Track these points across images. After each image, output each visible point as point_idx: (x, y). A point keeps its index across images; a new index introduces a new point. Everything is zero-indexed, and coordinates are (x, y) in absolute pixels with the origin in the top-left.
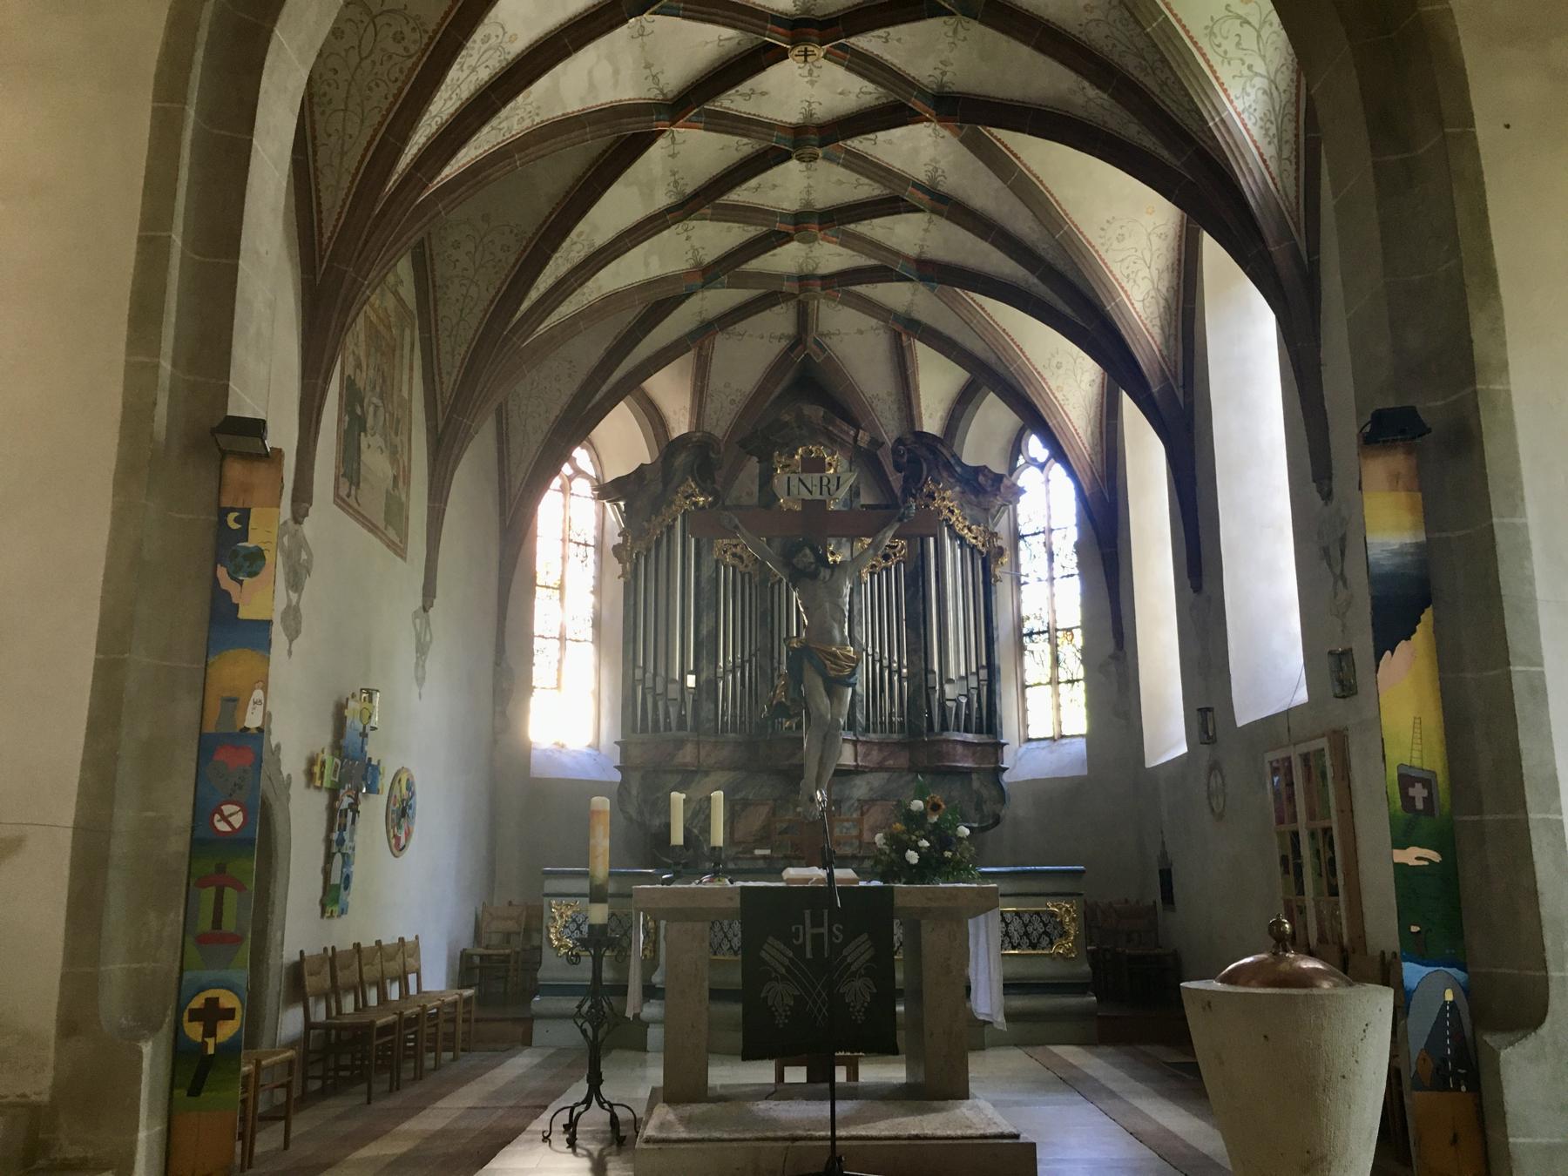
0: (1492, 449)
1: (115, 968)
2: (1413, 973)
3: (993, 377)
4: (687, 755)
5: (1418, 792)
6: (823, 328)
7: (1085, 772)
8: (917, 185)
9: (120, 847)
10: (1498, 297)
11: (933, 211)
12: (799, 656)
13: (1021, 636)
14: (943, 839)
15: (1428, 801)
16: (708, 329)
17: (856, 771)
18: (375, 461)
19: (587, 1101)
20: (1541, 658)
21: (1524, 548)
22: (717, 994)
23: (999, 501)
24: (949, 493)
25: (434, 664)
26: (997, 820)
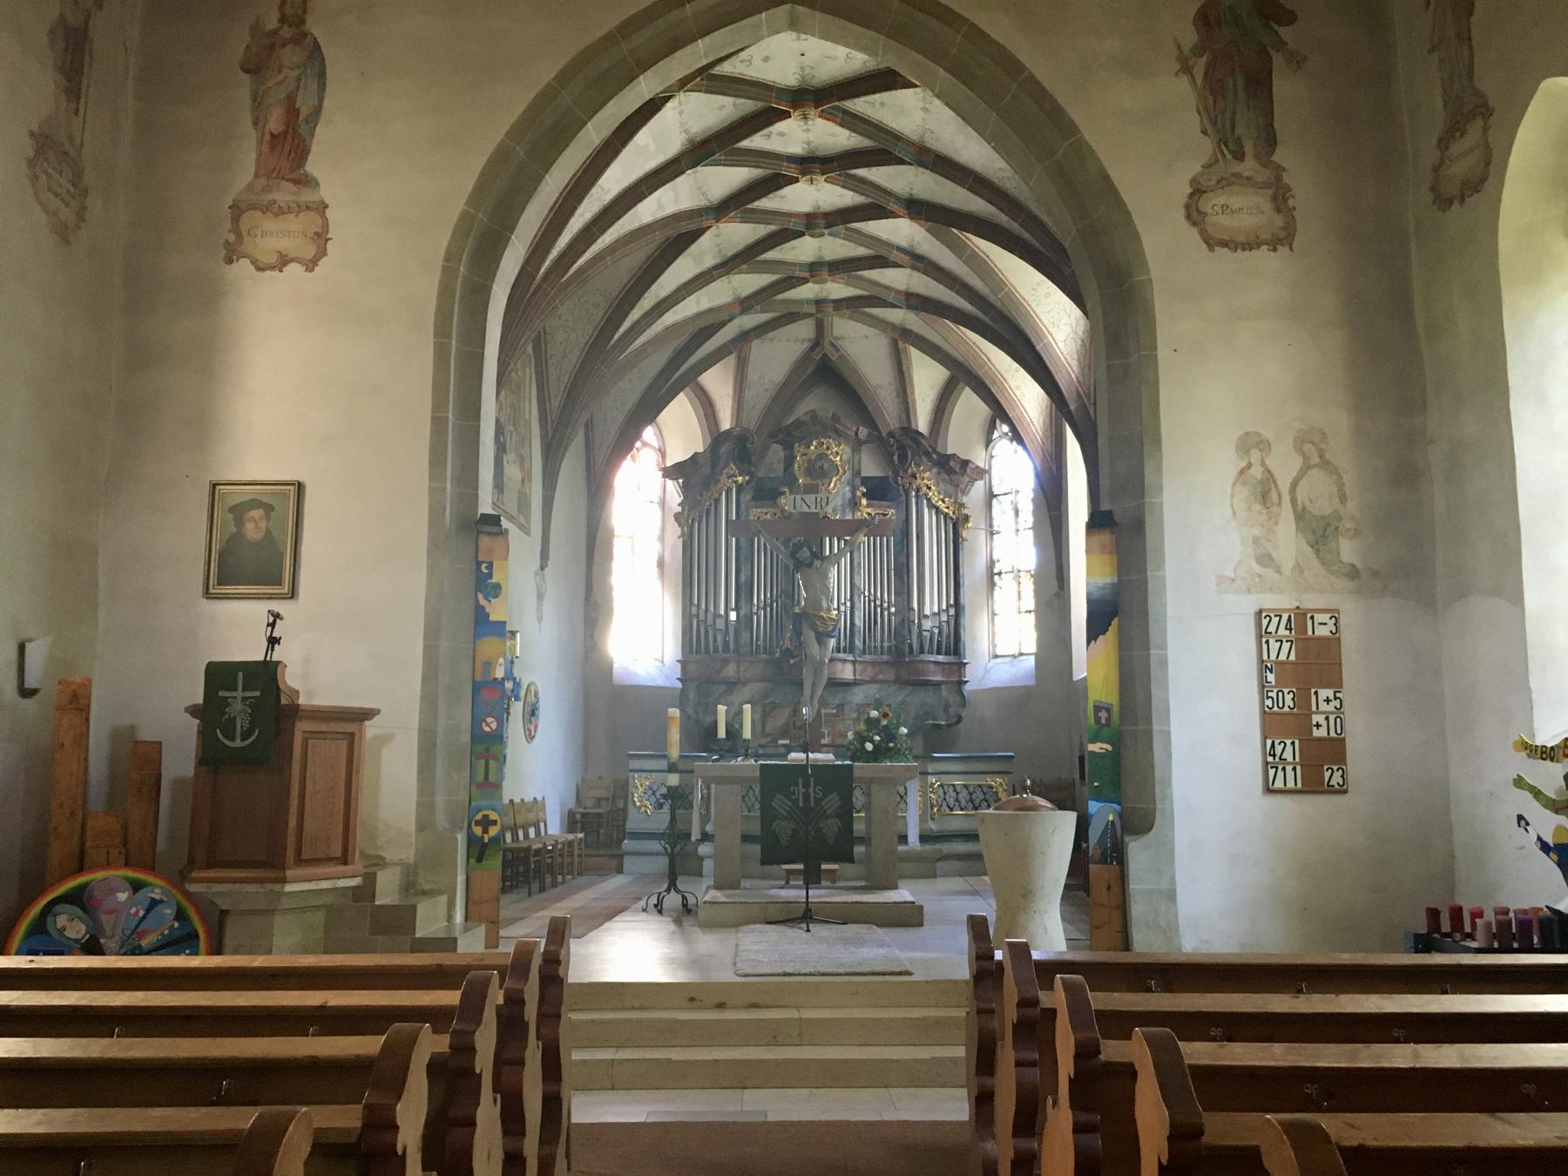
1: (440, 799)
2: (1093, 806)
3: (964, 375)
4: (730, 671)
5: (1103, 714)
6: (836, 333)
7: (1032, 682)
8: (900, 249)
9: (440, 739)
10: (1160, 451)
11: (914, 268)
12: (804, 615)
13: (992, 575)
15: (1108, 719)
16: (745, 337)
17: (855, 683)
18: (513, 472)
19: (668, 890)
20: (1165, 642)
21: (1163, 589)
22: (746, 838)
23: (966, 479)
24: (927, 474)
25: (548, 606)
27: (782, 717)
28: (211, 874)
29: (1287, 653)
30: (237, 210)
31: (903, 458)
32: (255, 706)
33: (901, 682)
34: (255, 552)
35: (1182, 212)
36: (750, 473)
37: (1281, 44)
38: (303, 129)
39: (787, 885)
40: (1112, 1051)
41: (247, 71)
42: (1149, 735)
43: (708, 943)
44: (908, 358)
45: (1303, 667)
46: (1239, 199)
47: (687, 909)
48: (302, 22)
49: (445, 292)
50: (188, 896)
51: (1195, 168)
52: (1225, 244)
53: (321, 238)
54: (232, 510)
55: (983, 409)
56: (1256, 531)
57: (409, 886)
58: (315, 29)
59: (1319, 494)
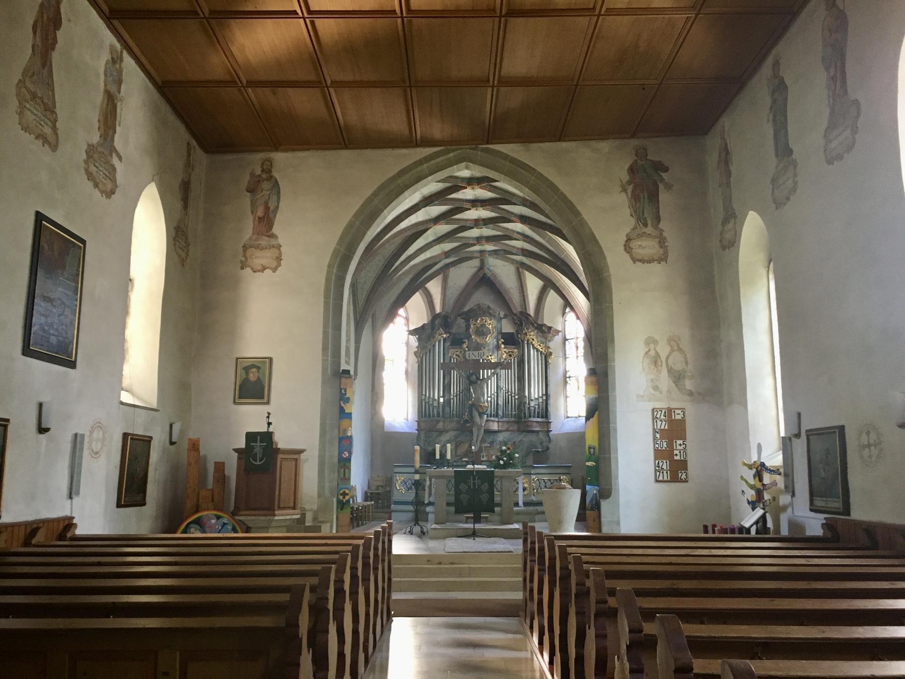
0: (610, 378)
1: (327, 485)
4: (440, 426)
5: (592, 450)
8: (518, 233)
9: (326, 460)
11: (524, 241)
12: (473, 405)
14: (510, 457)
16: (447, 266)
17: (498, 431)
21: (615, 401)
22: (448, 504)
26: (548, 449)
27: (463, 449)
28: (247, 512)
29: (664, 426)
30: (245, 248)
31: (521, 324)
32: (265, 449)
33: (520, 431)
34: (253, 386)
35: (623, 248)
36: (450, 333)
37: (662, 180)
38: (271, 215)
39: (466, 522)
40: (649, 628)
41: (248, 191)
42: (610, 458)
43: (433, 544)
44: (524, 275)
45: (671, 431)
46: (645, 242)
47: (423, 533)
48: (271, 171)
49: (328, 280)
50: (235, 520)
51: (628, 230)
52: (640, 261)
53: (279, 259)
54: (244, 369)
55: (560, 301)
56: (652, 377)
57: (315, 519)
58: (276, 174)
59: (677, 361)
